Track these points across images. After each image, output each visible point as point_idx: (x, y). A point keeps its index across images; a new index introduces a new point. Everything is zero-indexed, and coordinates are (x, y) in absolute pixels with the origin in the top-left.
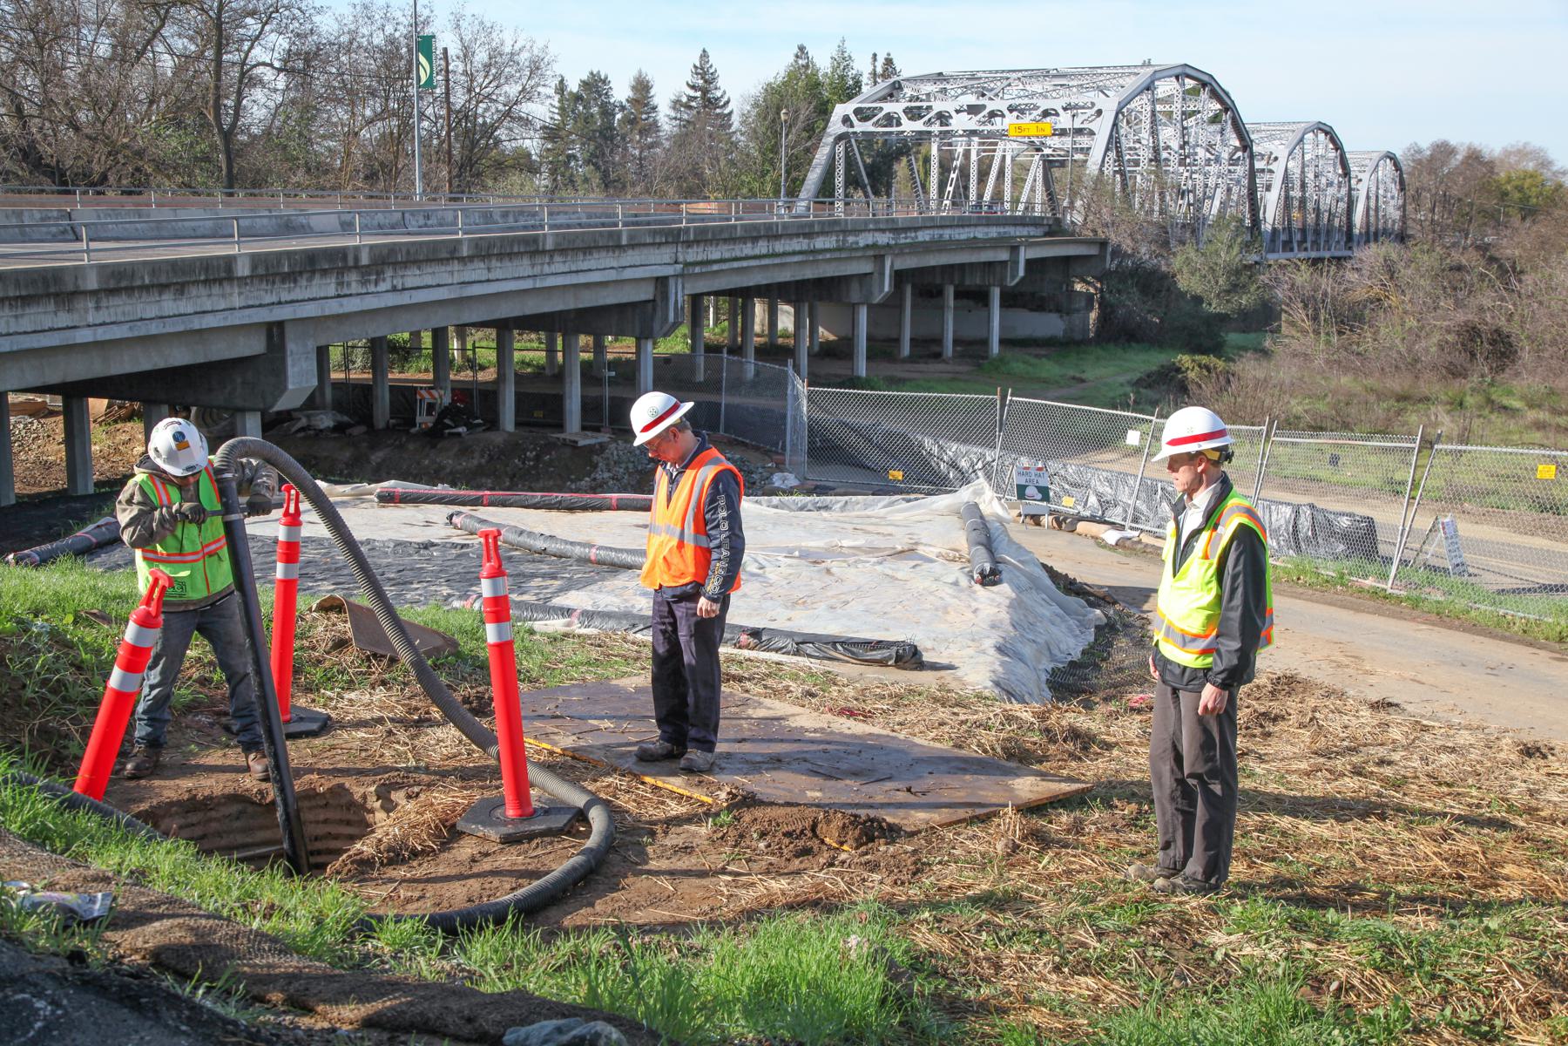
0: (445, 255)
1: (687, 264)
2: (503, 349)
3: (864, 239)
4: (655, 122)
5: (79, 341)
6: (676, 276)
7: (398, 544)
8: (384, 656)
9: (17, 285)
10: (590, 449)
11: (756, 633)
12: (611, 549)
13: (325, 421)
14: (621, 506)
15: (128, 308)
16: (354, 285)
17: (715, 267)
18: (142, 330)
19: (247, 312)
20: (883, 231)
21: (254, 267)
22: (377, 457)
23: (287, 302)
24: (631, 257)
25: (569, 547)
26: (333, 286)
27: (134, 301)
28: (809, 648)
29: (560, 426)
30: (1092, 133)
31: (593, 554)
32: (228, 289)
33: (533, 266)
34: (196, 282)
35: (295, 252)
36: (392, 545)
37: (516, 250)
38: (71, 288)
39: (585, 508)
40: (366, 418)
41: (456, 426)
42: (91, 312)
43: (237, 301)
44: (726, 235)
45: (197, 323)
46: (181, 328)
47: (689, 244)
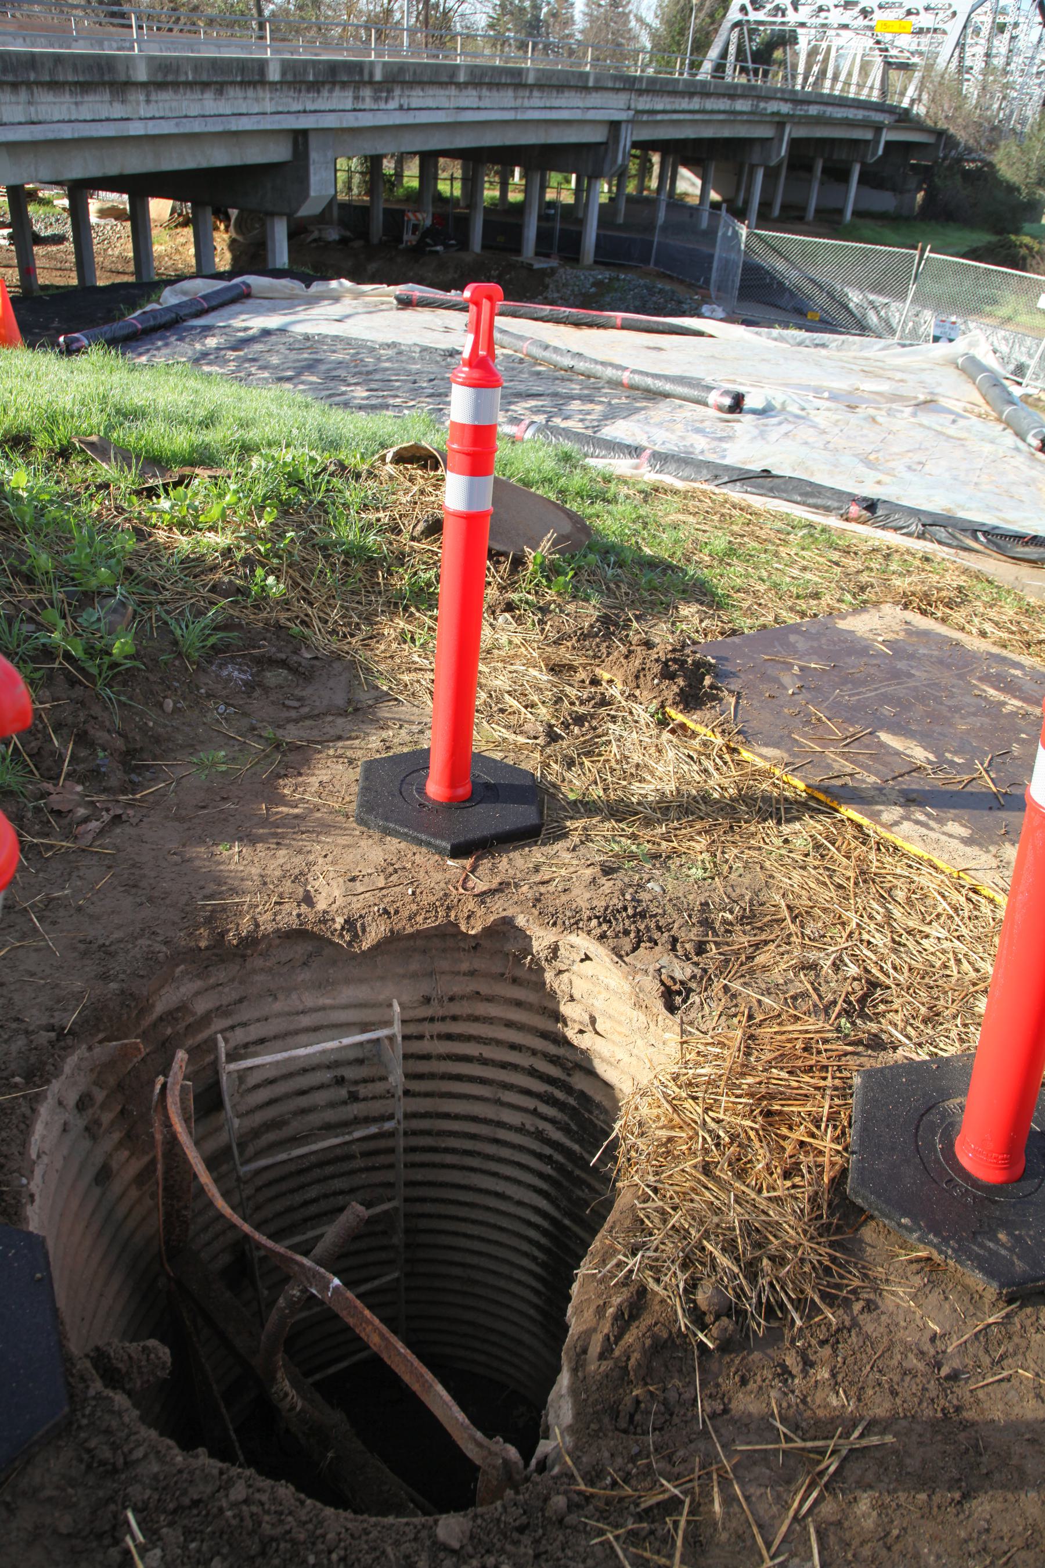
0: (445, 79)
1: (638, 112)
2: (472, 184)
3: (772, 107)
4: (572, 17)
5: (132, 133)
6: (627, 122)
7: (424, 349)
8: (505, 554)
9: (75, 70)
10: (543, 272)
11: (871, 506)
12: (647, 374)
13: (333, 234)
14: (626, 326)
15: (174, 104)
16: (368, 100)
17: (659, 117)
18: (187, 127)
19: (277, 117)
20: (786, 100)
21: (284, 73)
22: (372, 267)
23: (311, 112)
24: (595, 99)
25: (599, 367)
26: (350, 100)
27: (179, 97)
28: (941, 533)
29: (518, 251)
30: (944, 32)
31: (626, 377)
32: (260, 93)
33: (516, 98)
34: (233, 83)
35: (319, 62)
36: (418, 349)
37: (503, 81)
38: (123, 78)
39: (590, 325)
40: (364, 234)
41: (436, 245)
42: (143, 105)
43: (269, 107)
44: (670, 88)
45: (236, 125)
46: (219, 128)
47: (641, 92)
